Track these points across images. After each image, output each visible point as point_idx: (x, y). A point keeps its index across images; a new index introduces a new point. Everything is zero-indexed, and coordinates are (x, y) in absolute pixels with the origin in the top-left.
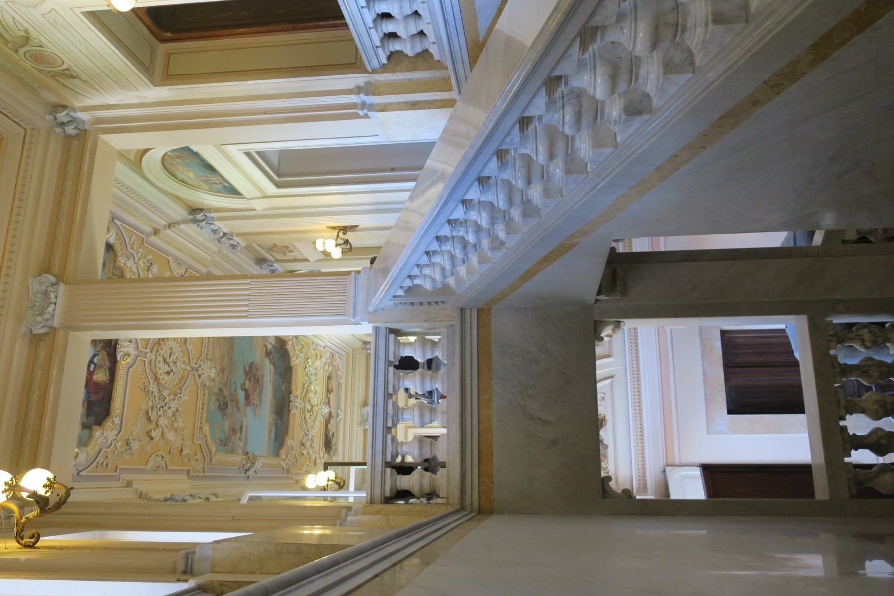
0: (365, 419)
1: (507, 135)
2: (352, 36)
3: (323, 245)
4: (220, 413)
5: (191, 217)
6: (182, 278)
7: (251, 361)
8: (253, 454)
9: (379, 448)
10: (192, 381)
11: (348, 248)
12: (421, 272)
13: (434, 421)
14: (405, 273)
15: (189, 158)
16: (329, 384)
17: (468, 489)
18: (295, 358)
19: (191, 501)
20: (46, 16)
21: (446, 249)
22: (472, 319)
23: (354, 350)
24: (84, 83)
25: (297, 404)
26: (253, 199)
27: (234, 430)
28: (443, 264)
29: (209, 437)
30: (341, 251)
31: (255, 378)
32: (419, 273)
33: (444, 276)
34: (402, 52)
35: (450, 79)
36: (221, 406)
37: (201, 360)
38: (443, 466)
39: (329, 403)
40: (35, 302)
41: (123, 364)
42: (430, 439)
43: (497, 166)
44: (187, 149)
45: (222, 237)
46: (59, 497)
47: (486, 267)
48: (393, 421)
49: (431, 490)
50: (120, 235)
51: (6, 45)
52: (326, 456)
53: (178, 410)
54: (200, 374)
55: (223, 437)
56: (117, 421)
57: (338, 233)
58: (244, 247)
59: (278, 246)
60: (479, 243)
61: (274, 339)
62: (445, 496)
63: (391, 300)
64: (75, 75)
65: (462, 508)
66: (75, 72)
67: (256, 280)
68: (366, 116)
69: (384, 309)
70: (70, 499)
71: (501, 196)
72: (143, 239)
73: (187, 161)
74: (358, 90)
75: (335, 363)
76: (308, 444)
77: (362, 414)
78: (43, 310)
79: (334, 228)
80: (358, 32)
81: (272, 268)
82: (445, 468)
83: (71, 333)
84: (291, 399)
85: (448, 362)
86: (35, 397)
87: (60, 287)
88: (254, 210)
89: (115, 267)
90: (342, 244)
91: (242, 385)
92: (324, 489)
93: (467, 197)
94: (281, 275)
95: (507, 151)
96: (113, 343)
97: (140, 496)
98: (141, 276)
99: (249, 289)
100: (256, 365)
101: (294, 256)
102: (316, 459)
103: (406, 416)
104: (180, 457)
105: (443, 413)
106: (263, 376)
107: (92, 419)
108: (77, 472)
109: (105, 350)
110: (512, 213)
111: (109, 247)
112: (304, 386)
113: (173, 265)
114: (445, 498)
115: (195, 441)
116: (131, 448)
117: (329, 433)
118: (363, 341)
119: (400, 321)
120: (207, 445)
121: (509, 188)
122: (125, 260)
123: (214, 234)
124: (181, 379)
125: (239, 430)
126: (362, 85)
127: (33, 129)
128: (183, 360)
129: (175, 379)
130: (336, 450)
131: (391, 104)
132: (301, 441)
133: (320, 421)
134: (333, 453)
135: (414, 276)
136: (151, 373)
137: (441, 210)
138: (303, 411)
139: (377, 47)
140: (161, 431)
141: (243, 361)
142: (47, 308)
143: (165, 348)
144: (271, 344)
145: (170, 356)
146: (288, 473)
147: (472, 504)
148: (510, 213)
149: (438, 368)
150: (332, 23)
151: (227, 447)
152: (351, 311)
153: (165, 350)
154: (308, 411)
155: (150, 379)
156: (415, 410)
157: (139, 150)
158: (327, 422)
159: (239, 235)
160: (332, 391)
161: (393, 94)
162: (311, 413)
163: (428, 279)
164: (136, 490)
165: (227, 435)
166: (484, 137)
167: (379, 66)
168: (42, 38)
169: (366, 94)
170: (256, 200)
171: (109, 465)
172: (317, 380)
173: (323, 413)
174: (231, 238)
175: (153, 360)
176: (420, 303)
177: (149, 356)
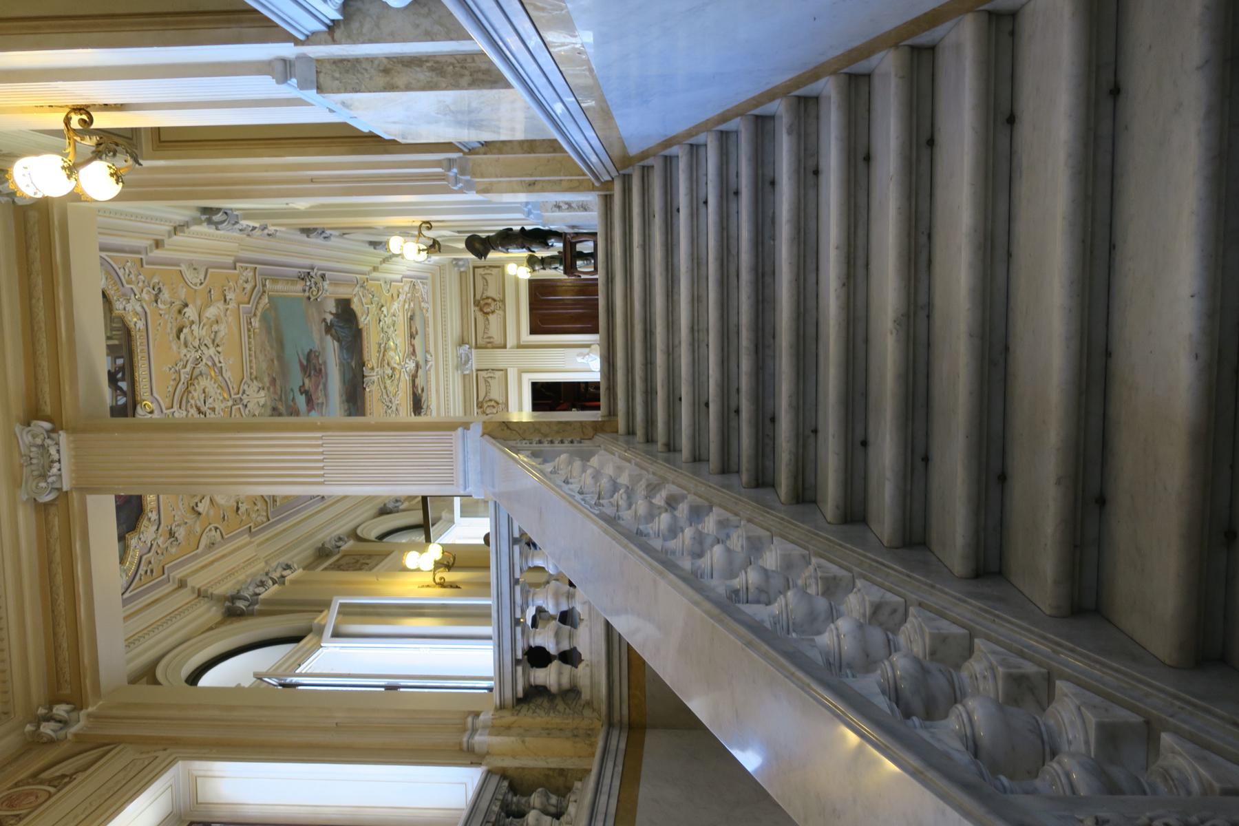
0: (463, 362)
7: (307, 351)
16: (412, 325)
18: (364, 317)
25: (373, 376)
31: (315, 370)
39: (414, 353)
49: (571, 685)
54: (245, 404)
56: (154, 516)
72: (141, 259)
84: (365, 374)
86: (59, 579)
97: (199, 595)
100: (315, 352)
106: (325, 363)
112: (380, 347)
113: (189, 275)
116: (177, 538)
117: (418, 390)
122: (124, 303)
130: (428, 407)
133: (406, 378)
141: (298, 355)
143: (196, 395)
145: (205, 403)
152: (461, 481)
160: (417, 333)
164: (193, 588)
171: (154, 571)
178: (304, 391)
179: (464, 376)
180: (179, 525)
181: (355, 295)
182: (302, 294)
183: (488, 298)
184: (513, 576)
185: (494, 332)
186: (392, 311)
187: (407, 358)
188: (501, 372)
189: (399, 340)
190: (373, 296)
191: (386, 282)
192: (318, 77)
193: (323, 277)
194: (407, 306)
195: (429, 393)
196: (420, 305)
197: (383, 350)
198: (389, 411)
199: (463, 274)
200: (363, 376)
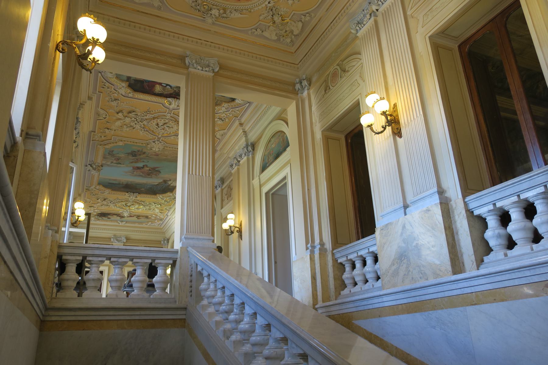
1: (297, 345)
2: (353, 242)
3: (231, 218)
4: (130, 152)
5: (249, 144)
6: (214, 136)
7: (161, 171)
8: (102, 169)
9: (97, 252)
10: (151, 137)
11: (230, 232)
12: (212, 282)
13: (112, 289)
14: (211, 272)
15: (283, 145)
16: (143, 217)
17: (60, 313)
19: (75, 132)
20: (356, 81)
21: (225, 300)
22: (179, 315)
23: (164, 233)
24: (322, 96)
25: (132, 197)
26: (259, 179)
27: (118, 159)
28: (216, 297)
29: (115, 144)
30: (227, 229)
31: (151, 173)
32: (211, 281)
33: (208, 298)
34: (344, 271)
35: (330, 301)
36: (134, 153)
37: (164, 143)
38: (80, 295)
39: (131, 216)
40: (204, 60)
41: (165, 101)
42: (99, 287)
43: (277, 337)
44: (288, 145)
45: (237, 160)
46: (86, 65)
47: (213, 326)
48: (114, 262)
49: (63, 286)
50: (240, 105)
51: (340, 61)
52: (95, 213)
53: (134, 128)
55: (114, 153)
56: (131, 95)
57: (238, 228)
58: (231, 172)
59: (231, 191)
60: (229, 322)
61: (174, 185)
62: (57, 296)
63: (194, 262)
64: (327, 92)
65: (47, 309)
66: (328, 92)
67: (211, 180)
68: (307, 249)
69: (189, 257)
70: (84, 71)
71: (258, 339)
72: (238, 117)
73: (281, 144)
74: (322, 244)
75: (156, 221)
76: (105, 202)
77: (121, 237)
78: (199, 63)
79: (241, 225)
80: (355, 246)
81: (218, 187)
82: (78, 296)
83: (185, 77)
84: (135, 194)
85: (151, 298)
87: (212, 74)
88: (253, 179)
89: (222, 101)
90: (231, 230)
91: (147, 165)
92: (73, 213)
93: (258, 316)
94: (213, 192)
95: (287, 344)
96: (178, 97)
97: (81, 104)
98: (216, 114)
99: (206, 175)
100: (159, 174)
101: (225, 200)
102: (94, 207)
103: (117, 271)
104: (104, 128)
105: (117, 296)
106: (151, 177)
107: (132, 82)
108: (101, 71)
109: (174, 92)
110: (247, 345)
111: (233, 100)
112: (143, 202)
113: (222, 132)
114: (56, 296)
115: (113, 137)
116: (113, 101)
117: (110, 216)
118: (170, 239)
119: (180, 268)
120: (110, 143)
121: (263, 344)
123: (239, 156)
124: (153, 131)
125: (118, 162)
126: (325, 247)
127: (298, 68)
128: (165, 133)
129: (154, 128)
130: (99, 220)
131: (315, 264)
132: (107, 199)
133: (120, 211)
134: (97, 218)
135: (210, 278)
136: (158, 116)
137: (251, 300)
138: (127, 201)
139: (347, 257)
140: (121, 118)
142: (200, 66)
143: (172, 124)
144: (171, 184)
145: (168, 127)
146: (86, 190)
147: (49, 316)
148: (247, 344)
149: (147, 291)
150: (360, 230)
151: (108, 155)
152: (189, 236)
153: (171, 124)
154: (126, 203)
155: (154, 115)
156: (121, 276)
157: (287, 119)
158: (118, 215)
159: (238, 169)
160: (138, 219)
161: (320, 265)
162: (125, 205)
163: (207, 287)
164: (86, 102)
165: (115, 155)
166: (295, 330)
167: (336, 258)
168: (345, 78)
169: (320, 249)
170: (258, 181)
171: (103, 89)
172: (146, 209)
173: (124, 213)
174: (237, 165)
175: (166, 117)
176: (192, 281)
177: (169, 115)
179: (110, 238)
180: (118, 104)
184: (112, 257)
187: (130, 213)
189: (136, 209)
190: (168, 202)
191: (170, 208)
192: (444, 203)
195: (105, 221)
196: (150, 222)
200: (134, 193)
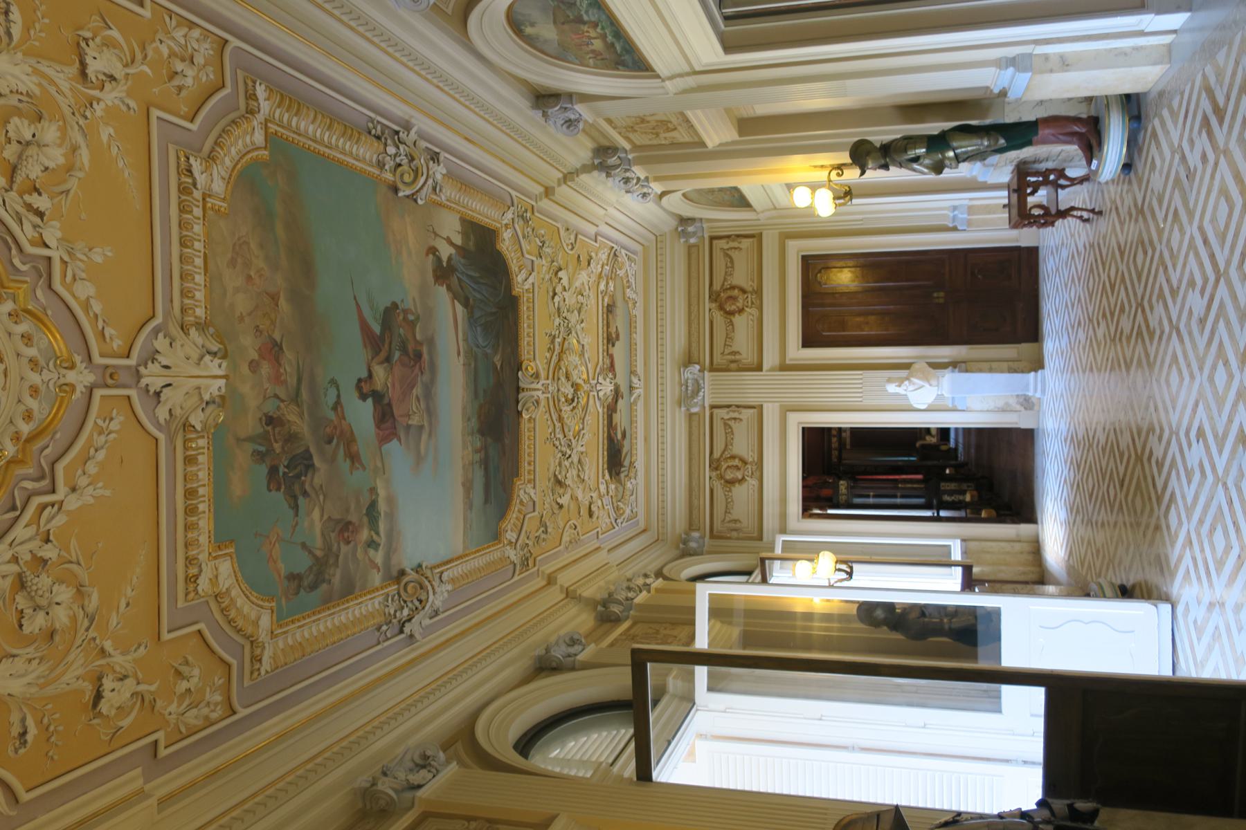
31: (404, 349)
84: (521, 385)
100: (406, 312)
106: (431, 342)
112: (553, 342)
117: (616, 434)
160: (618, 338)
178: (365, 388)
179: (690, 416)
181: (506, 225)
182: (376, 171)
183: (733, 288)
185: (743, 342)
186: (577, 284)
188: (752, 411)
189: (588, 337)
193: (435, 157)
194: (602, 287)
196: (624, 293)
197: (557, 349)
198: (567, 463)
199: (694, 250)
200: (518, 390)
